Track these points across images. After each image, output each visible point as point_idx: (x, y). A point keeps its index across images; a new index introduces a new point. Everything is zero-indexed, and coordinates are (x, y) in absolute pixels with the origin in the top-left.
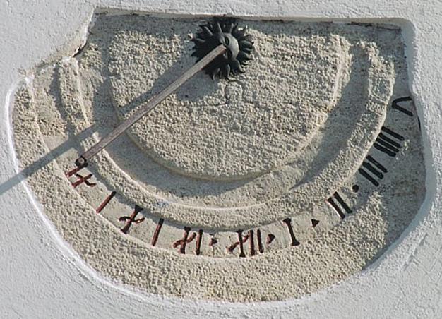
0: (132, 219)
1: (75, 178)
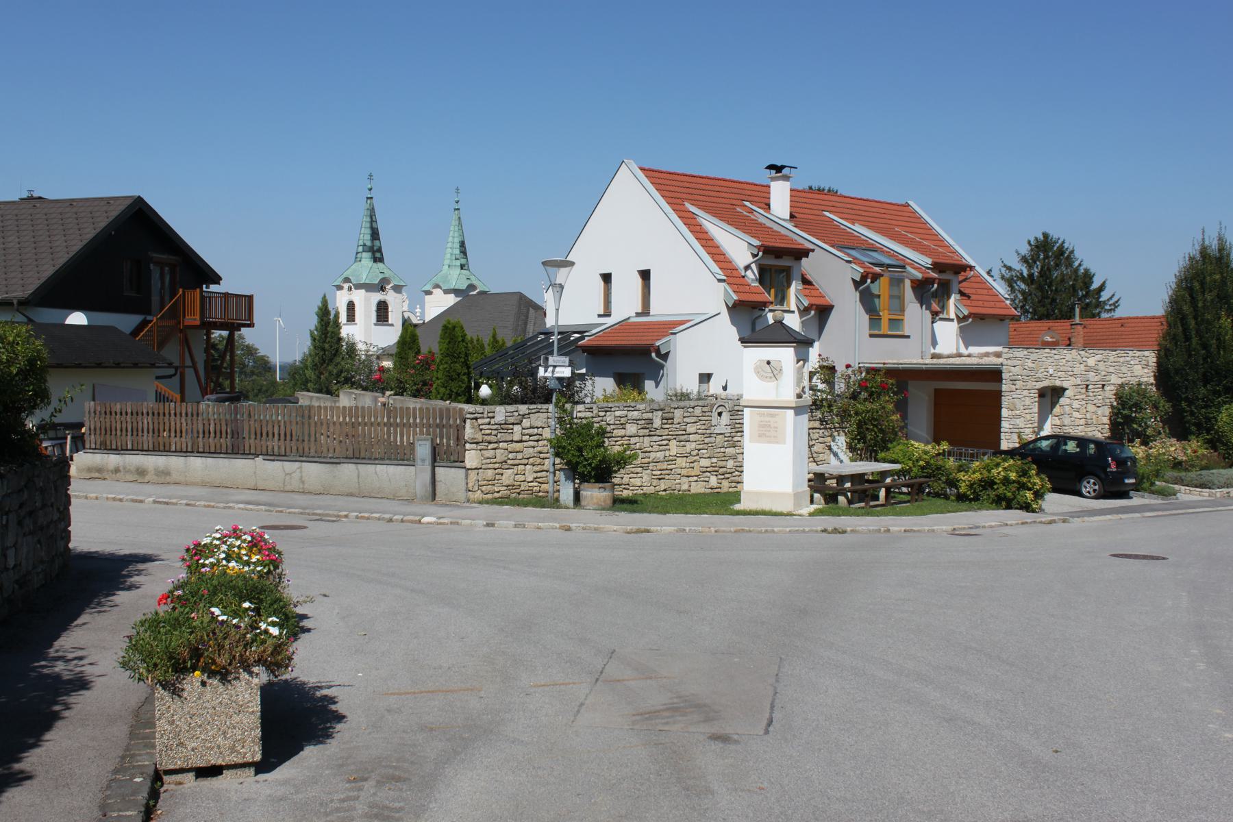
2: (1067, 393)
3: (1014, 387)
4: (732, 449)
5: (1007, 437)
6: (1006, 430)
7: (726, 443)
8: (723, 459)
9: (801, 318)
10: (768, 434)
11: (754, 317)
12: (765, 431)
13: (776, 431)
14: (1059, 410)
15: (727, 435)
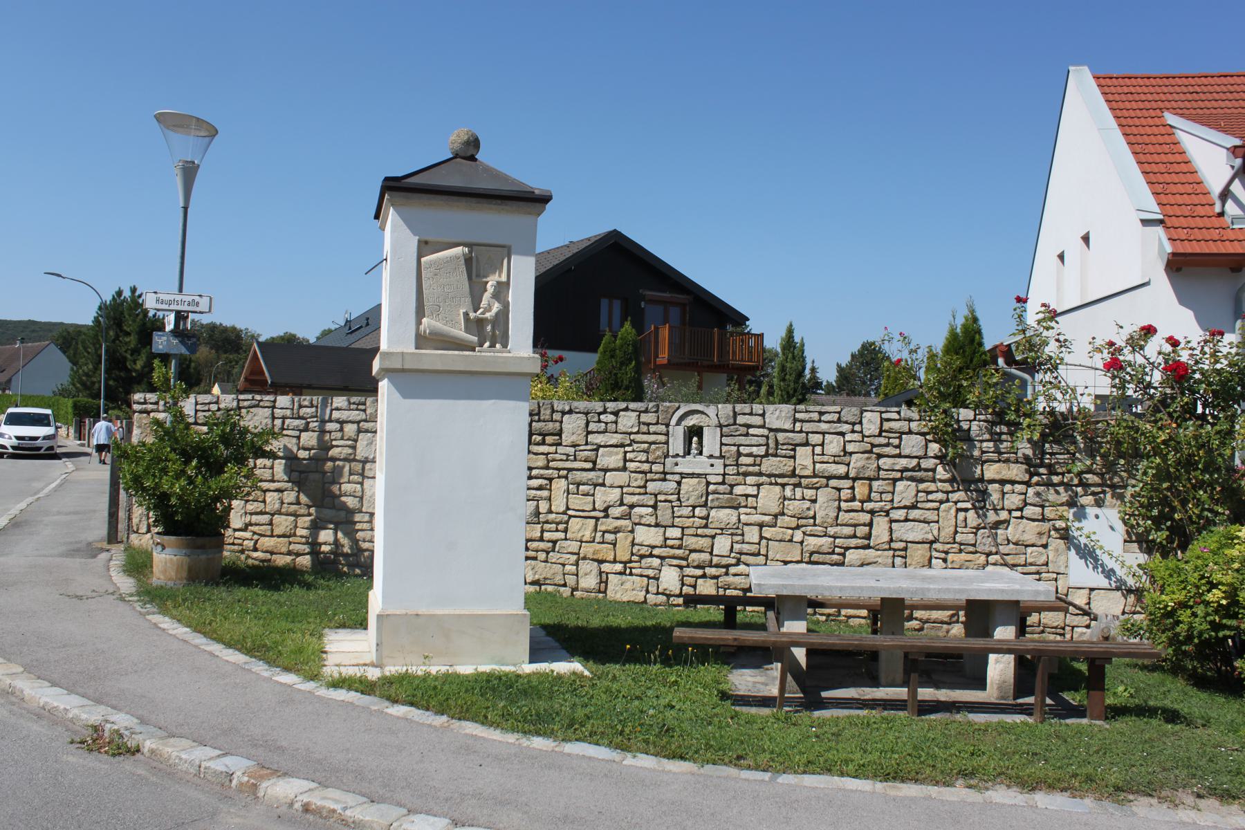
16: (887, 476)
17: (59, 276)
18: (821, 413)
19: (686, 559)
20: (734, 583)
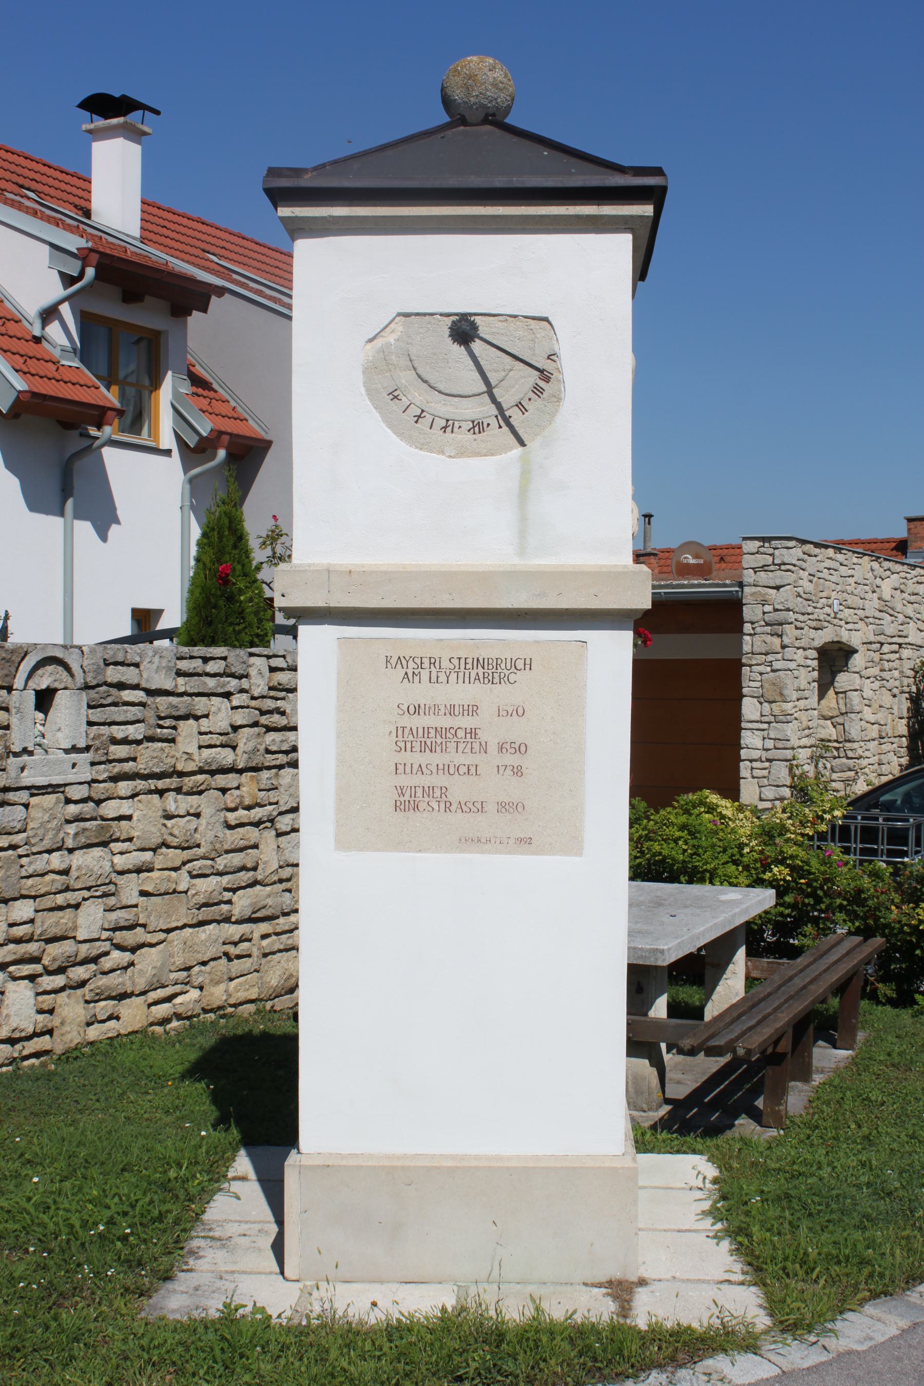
0: (419, 417)
1: (391, 397)
2: (857, 661)
3: (776, 641)
4: (97, 852)
5: (757, 773)
6: (755, 754)
7: (71, 829)
8: (60, 899)
9: (186, 470)
10: (459, 789)
11: (68, 455)
12: (446, 769)
13: (518, 771)
14: (833, 704)
15: (76, 793)
16: (274, 763)
17: (679, 1231)
18: (206, 660)
19: (36, 960)
20: (108, 988)
